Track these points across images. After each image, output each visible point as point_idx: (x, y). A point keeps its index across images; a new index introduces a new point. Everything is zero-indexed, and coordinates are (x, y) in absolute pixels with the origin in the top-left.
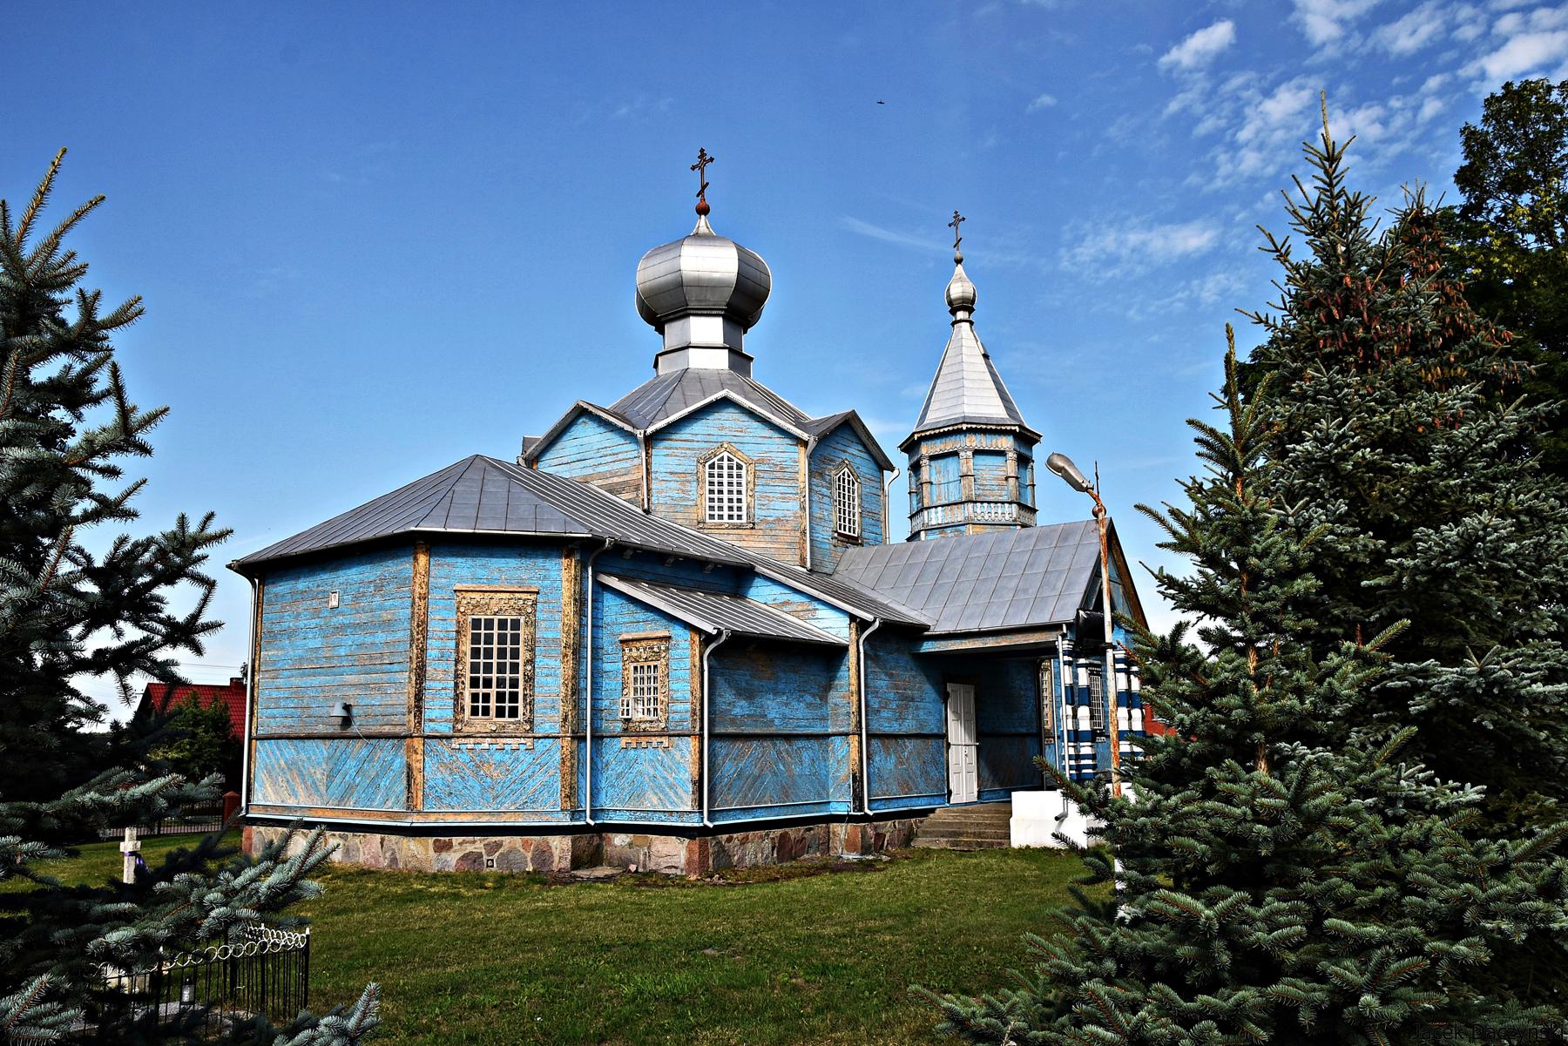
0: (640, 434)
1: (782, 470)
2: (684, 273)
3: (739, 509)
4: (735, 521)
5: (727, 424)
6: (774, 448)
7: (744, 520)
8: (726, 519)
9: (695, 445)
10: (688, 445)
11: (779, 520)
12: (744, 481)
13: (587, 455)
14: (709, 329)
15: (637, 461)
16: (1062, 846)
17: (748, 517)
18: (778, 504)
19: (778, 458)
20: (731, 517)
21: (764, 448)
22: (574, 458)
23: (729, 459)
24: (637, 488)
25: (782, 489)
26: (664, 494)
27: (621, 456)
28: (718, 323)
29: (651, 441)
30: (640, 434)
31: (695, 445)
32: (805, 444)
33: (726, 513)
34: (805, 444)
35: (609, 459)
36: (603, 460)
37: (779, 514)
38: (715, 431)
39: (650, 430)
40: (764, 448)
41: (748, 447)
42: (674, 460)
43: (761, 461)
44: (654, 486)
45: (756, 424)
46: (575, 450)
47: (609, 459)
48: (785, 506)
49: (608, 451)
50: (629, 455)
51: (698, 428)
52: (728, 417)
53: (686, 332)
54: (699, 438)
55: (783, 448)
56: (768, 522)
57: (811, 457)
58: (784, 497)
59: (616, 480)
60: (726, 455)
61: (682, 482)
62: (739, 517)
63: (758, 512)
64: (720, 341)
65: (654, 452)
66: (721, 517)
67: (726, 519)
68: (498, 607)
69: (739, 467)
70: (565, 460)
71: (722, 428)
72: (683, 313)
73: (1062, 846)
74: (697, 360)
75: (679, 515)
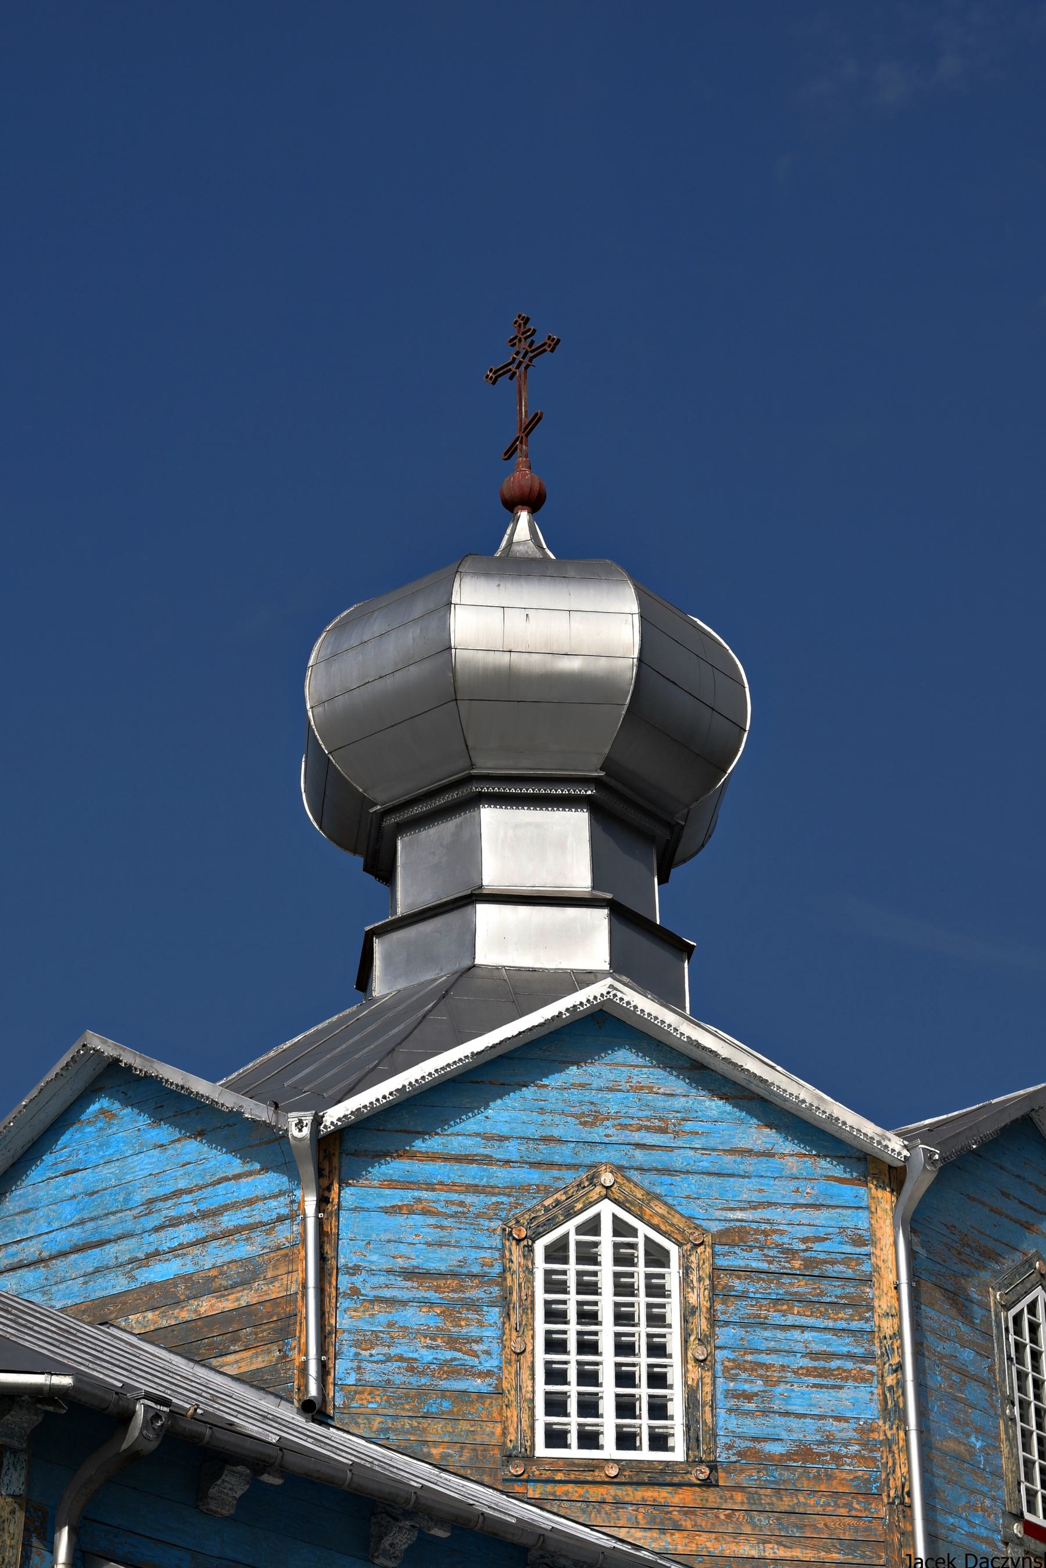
0: (298, 1128)
1: (813, 1269)
2: (460, 656)
3: (658, 1410)
4: (645, 1454)
5: (612, 1103)
6: (780, 1190)
7: (678, 1453)
8: (609, 1450)
9: (501, 1175)
10: (471, 1173)
11: (804, 1452)
12: (674, 1313)
13: (110, 1227)
14: (536, 845)
15: (284, 1233)
16: (215, 1362)
17: (692, 1440)
18: (800, 1396)
19: (793, 1225)
20: (626, 1440)
21: (746, 1190)
22: (63, 1239)
23: (620, 1228)
24: (284, 1324)
25: (815, 1341)
26: (383, 1341)
27: (228, 1220)
28: (575, 824)
29: (337, 1156)
30: (298, 1128)
31: (501, 1175)
32: (893, 1176)
33: (608, 1422)
34: (893, 1176)
35: (186, 1233)
36: (169, 1239)
37: (807, 1431)
38: (566, 1129)
39: (333, 1115)
40: (746, 1190)
41: (686, 1186)
42: (416, 1228)
43: (734, 1236)
44: (342, 1320)
45: (715, 1106)
46: (68, 1212)
47: (186, 1233)
48: (826, 1400)
49: (186, 1206)
50: (261, 1213)
51: (505, 1112)
52: (621, 1069)
53: (469, 851)
54: (512, 1150)
55: (810, 1191)
56: (765, 1461)
57: (915, 1225)
58: (823, 1371)
59: (207, 1306)
60: (607, 1210)
61: (450, 1311)
62: (659, 1441)
63: (726, 1423)
64: (580, 878)
65: (348, 1196)
66: (589, 1439)
67: (609, 1450)
68: (671, 1442)
69: (657, 1257)
70: (31, 1250)
71: (595, 1118)
72: (462, 793)
73: (215, 1362)
74: (501, 939)
75: (436, 1430)
